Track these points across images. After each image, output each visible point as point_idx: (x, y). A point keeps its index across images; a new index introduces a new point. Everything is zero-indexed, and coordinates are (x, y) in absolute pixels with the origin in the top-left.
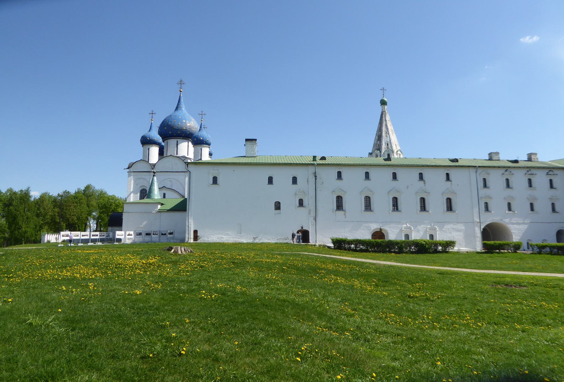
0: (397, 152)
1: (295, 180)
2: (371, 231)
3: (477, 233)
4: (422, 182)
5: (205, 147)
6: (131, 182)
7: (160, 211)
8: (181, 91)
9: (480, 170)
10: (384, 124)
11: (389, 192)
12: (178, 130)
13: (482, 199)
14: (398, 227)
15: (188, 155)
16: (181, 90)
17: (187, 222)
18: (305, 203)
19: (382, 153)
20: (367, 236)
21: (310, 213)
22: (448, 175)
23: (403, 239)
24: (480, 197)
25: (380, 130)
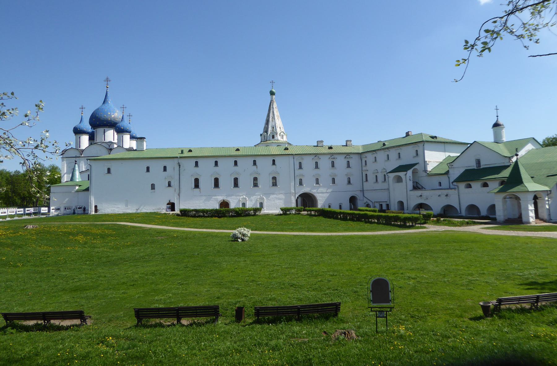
0: (280, 133)
1: (165, 169)
2: (218, 201)
3: (292, 201)
4: (255, 167)
5: (127, 134)
6: (65, 165)
7: (78, 191)
8: (107, 87)
9: (296, 157)
10: (271, 111)
11: (231, 175)
12: (104, 121)
13: (297, 177)
14: (237, 198)
15: (114, 140)
16: (108, 86)
17: (90, 200)
18: (172, 184)
19: (268, 135)
20: (217, 207)
21: (175, 191)
22: (274, 161)
23: (241, 206)
24: (296, 176)
25: (268, 116)
